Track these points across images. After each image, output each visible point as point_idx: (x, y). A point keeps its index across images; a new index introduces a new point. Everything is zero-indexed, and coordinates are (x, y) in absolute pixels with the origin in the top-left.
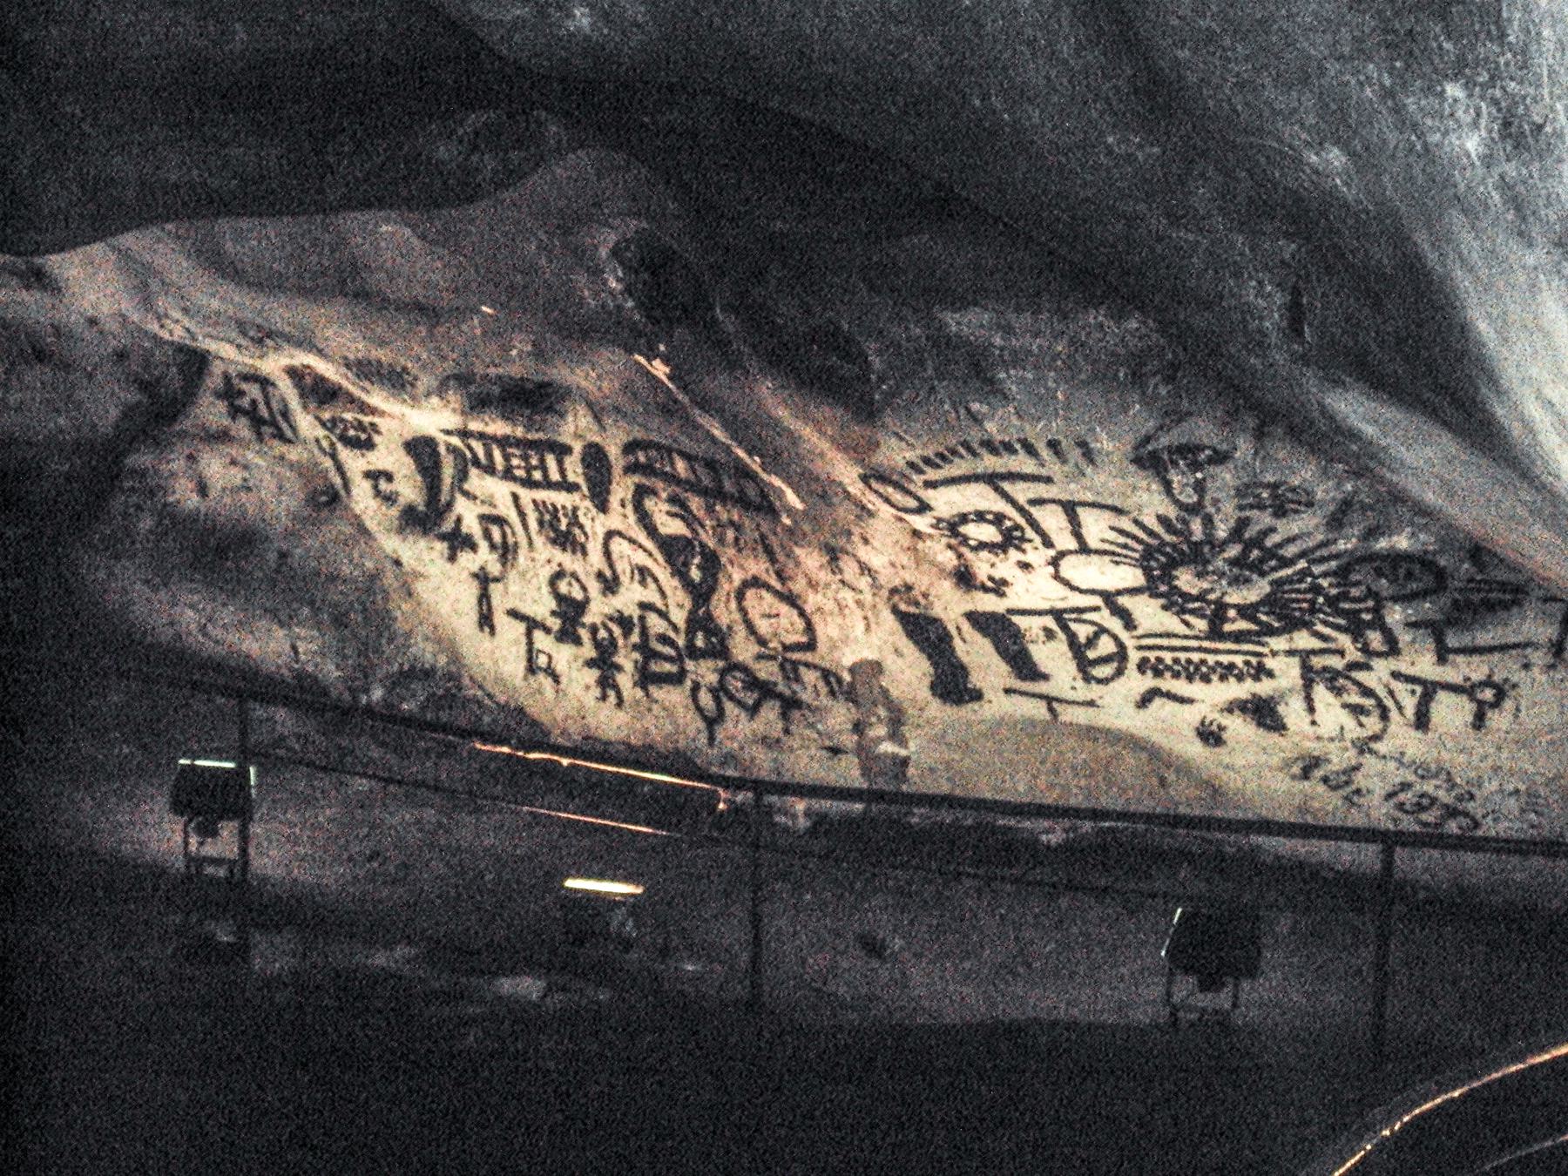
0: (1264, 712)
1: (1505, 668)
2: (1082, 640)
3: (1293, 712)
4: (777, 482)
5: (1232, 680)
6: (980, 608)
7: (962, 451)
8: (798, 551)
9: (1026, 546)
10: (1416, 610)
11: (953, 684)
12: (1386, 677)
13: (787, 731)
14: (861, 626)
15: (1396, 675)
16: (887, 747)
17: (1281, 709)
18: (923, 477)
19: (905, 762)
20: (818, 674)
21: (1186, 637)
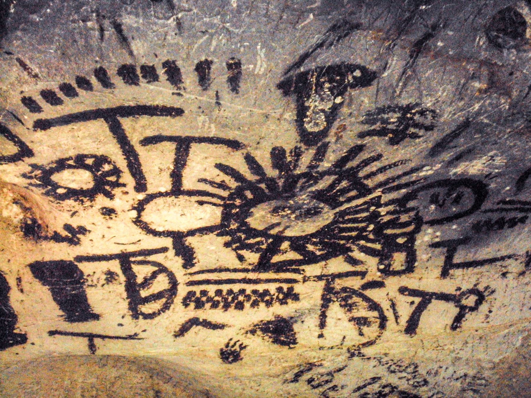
0: (281, 331)
1: (487, 278)
2: (140, 280)
3: (306, 331)
5: (262, 305)
7: (94, 80)
9: (117, 191)
10: (443, 232)
12: (394, 293)
15: (403, 290)
17: (296, 327)
18: (37, 116)
21: (235, 270)
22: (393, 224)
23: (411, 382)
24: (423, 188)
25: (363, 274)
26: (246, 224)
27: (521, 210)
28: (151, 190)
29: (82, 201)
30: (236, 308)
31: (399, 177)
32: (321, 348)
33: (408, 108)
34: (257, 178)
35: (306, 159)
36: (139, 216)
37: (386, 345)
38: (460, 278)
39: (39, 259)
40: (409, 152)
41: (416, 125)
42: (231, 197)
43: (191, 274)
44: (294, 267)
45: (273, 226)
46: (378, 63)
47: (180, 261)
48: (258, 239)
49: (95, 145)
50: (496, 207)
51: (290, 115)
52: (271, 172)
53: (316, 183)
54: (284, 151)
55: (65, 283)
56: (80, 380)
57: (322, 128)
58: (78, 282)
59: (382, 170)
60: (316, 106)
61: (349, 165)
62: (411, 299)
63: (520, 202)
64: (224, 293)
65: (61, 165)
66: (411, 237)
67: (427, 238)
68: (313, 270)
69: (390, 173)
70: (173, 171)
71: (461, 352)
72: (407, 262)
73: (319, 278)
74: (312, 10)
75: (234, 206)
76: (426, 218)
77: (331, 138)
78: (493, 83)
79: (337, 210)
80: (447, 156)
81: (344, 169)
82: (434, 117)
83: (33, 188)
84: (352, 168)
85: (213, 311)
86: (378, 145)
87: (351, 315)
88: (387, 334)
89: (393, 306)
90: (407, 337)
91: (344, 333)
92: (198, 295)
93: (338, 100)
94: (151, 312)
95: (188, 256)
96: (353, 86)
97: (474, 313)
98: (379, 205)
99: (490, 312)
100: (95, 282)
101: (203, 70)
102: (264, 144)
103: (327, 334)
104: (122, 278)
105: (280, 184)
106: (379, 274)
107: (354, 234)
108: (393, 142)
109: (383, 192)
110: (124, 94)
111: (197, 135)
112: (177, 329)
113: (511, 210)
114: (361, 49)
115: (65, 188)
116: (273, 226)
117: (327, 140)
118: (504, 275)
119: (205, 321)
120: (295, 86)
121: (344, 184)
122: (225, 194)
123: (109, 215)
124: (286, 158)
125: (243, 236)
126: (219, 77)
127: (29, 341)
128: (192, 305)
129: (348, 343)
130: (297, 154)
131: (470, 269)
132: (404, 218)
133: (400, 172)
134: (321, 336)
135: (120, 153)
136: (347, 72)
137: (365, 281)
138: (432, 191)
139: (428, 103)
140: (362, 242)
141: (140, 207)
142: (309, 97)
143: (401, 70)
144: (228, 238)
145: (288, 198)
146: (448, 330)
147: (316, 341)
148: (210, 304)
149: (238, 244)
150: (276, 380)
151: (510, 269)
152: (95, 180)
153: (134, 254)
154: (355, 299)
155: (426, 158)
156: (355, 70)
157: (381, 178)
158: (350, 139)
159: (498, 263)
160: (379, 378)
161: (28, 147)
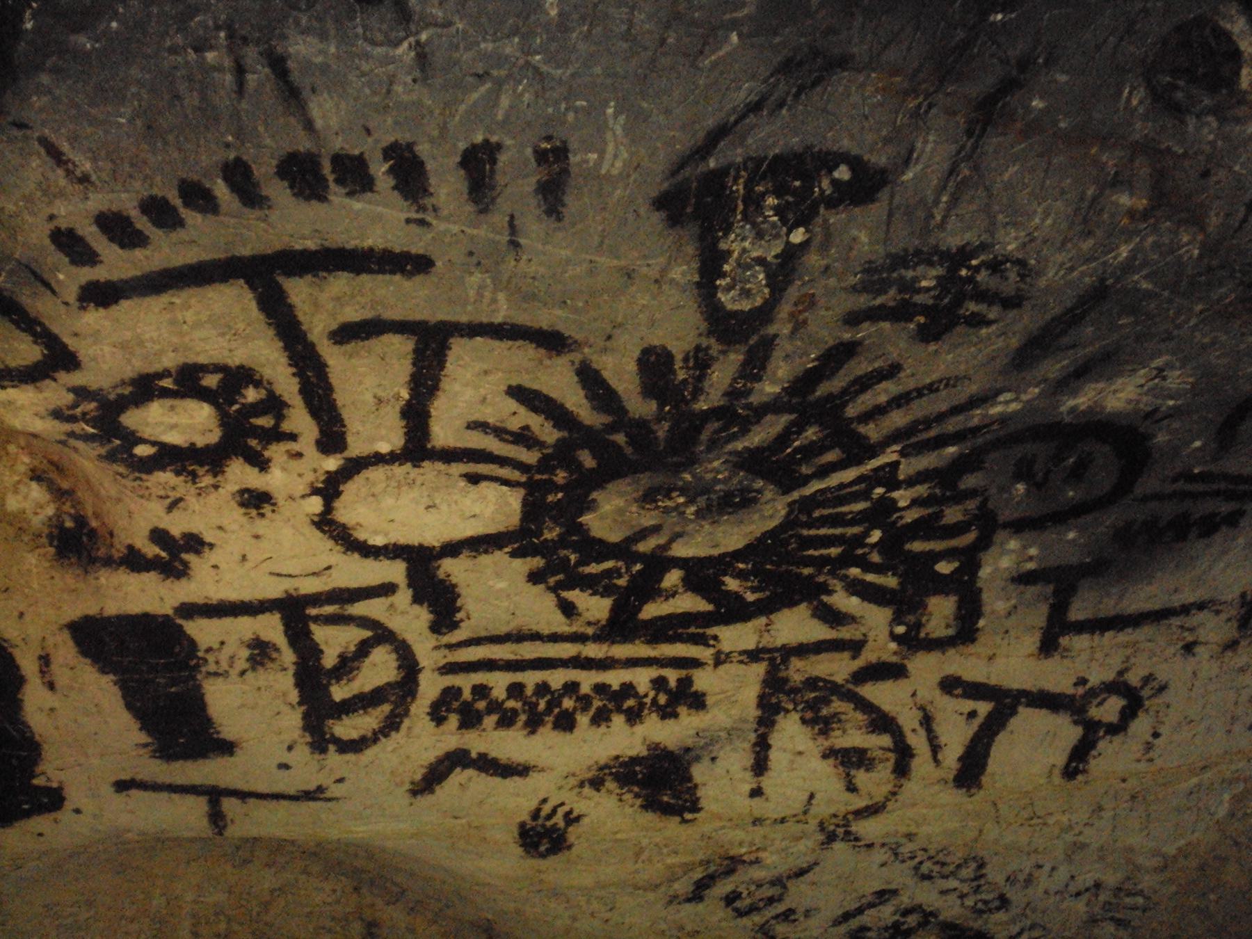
0: (662, 782)
1: (1149, 656)
2: (329, 660)
3: (721, 782)
5: (618, 720)
7: (221, 190)
9: (276, 452)
15: (950, 685)
17: (699, 772)
18: (87, 274)
21: (555, 638)
23: (969, 902)
24: (998, 444)
25: (855, 647)
27: (1229, 496)
28: (357, 447)
29: (194, 476)
31: (941, 417)
32: (757, 821)
35: (721, 376)
36: (328, 508)
37: (910, 813)
38: (1085, 656)
39: (93, 610)
40: (962, 359)
41: (983, 296)
42: (545, 464)
43: (450, 647)
44: (692, 630)
45: (643, 534)
46: (890, 150)
47: (423, 616)
48: (609, 564)
49: (222, 342)
50: (1169, 488)
51: (684, 272)
52: (639, 406)
53: (745, 431)
54: (669, 356)
55: (155, 669)
56: (189, 897)
57: (759, 301)
59: (900, 401)
60: (744, 250)
61: (822, 390)
62: (969, 705)
63: (1225, 477)
64: (529, 691)
65: (145, 388)
66: (970, 560)
68: (737, 637)
69: (920, 409)
70: (409, 403)
73: (753, 656)
75: (552, 487)
76: (1005, 515)
77: (780, 327)
79: (795, 495)
80: (1053, 368)
81: (811, 398)
82: (1022, 277)
83: (80, 444)
84: (830, 397)
85: (502, 733)
86: (891, 341)
87: (827, 744)
88: (912, 787)
89: (927, 721)
92: (467, 694)
93: (798, 236)
94: (355, 735)
95: (442, 603)
96: (832, 203)
97: (1118, 739)
99: (1156, 735)
100: (224, 665)
101: (478, 165)
102: (622, 339)
104: (288, 656)
105: (661, 434)
106: (893, 646)
107: (834, 551)
108: (928, 335)
109: (903, 453)
110: (293, 223)
111: (464, 319)
112: (418, 777)
113: (1204, 495)
114: (850, 117)
115: (154, 443)
116: (643, 534)
117: (771, 330)
118: (1189, 648)
120: (695, 204)
122: (530, 457)
123: (258, 507)
124: (674, 372)
125: (573, 558)
126: (517, 180)
127: (69, 805)
128: (454, 720)
129: (821, 809)
130: (701, 362)
132: (953, 515)
133: (944, 407)
134: (757, 792)
135: (284, 360)
137: (859, 663)
138: (1018, 451)
139: (1010, 244)
140: (855, 571)
141: (330, 489)
142: (728, 229)
143: (946, 166)
144: (537, 562)
145: (678, 468)
146: (1057, 779)
147: (744, 804)
148: (494, 718)
149: (561, 577)
150: (651, 896)
151: (1202, 634)
154: (837, 705)
156: (836, 166)
157: (898, 419)
158: (825, 328)
159: (1176, 621)
160: (895, 892)
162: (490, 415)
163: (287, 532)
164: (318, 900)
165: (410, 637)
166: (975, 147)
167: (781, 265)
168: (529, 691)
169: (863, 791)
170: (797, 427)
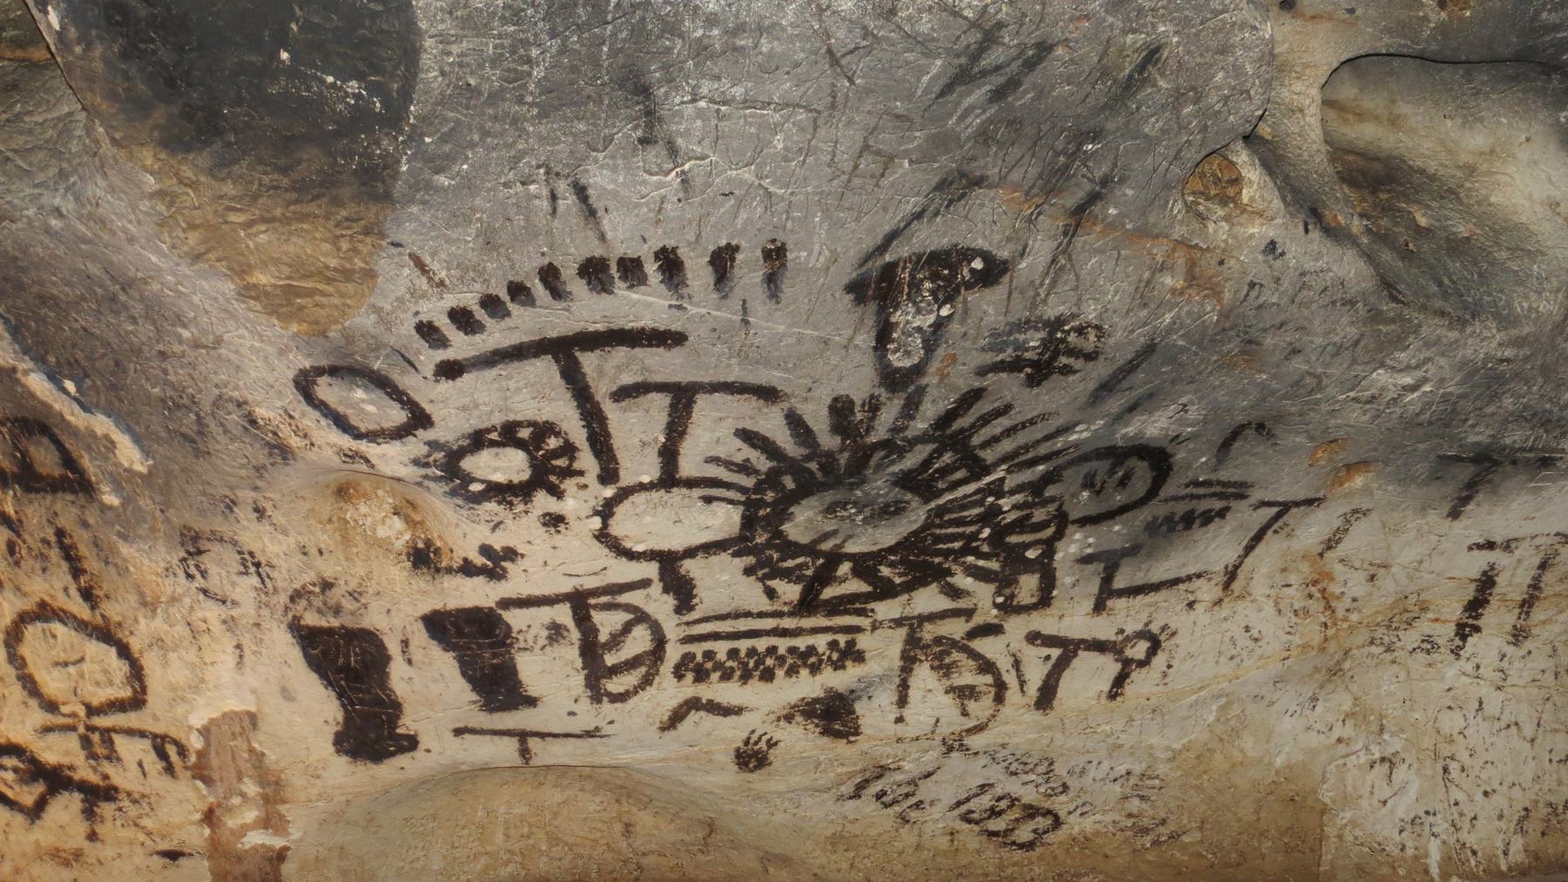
0: (833, 716)
1: (1163, 610)
3: (875, 714)
4: (101, 424)
5: (804, 672)
6: (453, 604)
8: (125, 550)
9: (569, 485)
11: (372, 729)
13: (92, 836)
14: (230, 659)
15: (1033, 638)
16: (256, 839)
17: (859, 707)
19: (281, 856)
20: (146, 744)
21: (761, 615)
22: (1020, 525)
23: (1042, 790)
24: (1072, 463)
25: (969, 613)
26: (779, 534)
27: (1221, 496)
28: (626, 479)
29: (511, 504)
30: (762, 678)
31: (1037, 443)
32: (899, 740)
33: (1058, 323)
34: (804, 451)
35: (888, 415)
36: (605, 525)
37: (1004, 729)
38: (1123, 613)
39: (439, 606)
40: (1056, 399)
41: (1071, 352)
42: (759, 488)
43: (688, 624)
44: (857, 605)
45: (826, 536)
46: (1011, 246)
47: (670, 601)
48: (800, 560)
49: (534, 403)
50: (1184, 492)
51: (866, 339)
52: (828, 441)
53: (901, 457)
54: (852, 403)
55: (480, 644)
56: (502, 810)
57: (916, 360)
58: (505, 645)
59: (1010, 432)
60: (908, 322)
61: (956, 426)
62: (1046, 651)
63: (1219, 483)
64: (743, 654)
65: (478, 441)
66: (1049, 547)
67: (1073, 549)
68: (886, 610)
69: (1022, 438)
70: (664, 445)
71: (1123, 736)
72: (1041, 589)
73: (898, 623)
74: (906, 154)
75: (761, 503)
76: (1074, 514)
77: (930, 379)
78: (1194, 278)
79: (933, 505)
80: (1115, 404)
81: (949, 432)
82: (1099, 338)
83: (431, 484)
84: (962, 430)
85: (724, 685)
86: (1009, 387)
87: (948, 683)
88: (1006, 710)
89: (1017, 664)
90: (1037, 716)
91: (936, 714)
92: (699, 658)
93: (945, 312)
94: (621, 690)
95: (682, 592)
96: (969, 286)
97: (1144, 670)
98: (1000, 494)
99: (1169, 667)
100: (530, 642)
101: (722, 261)
102: (817, 392)
103: (912, 715)
104: (575, 635)
105: (843, 462)
106: (995, 612)
107: (957, 545)
108: (1033, 382)
109: (1009, 471)
110: (588, 310)
111: (707, 380)
112: (666, 718)
113: (1205, 496)
114: (982, 225)
115: (483, 482)
116: (826, 536)
117: (924, 381)
118: (1191, 605)
119: (710, 702)
120: (877, 288)
121: (948, 458)
122: (748, 482)
123: (555, 526)
124: (853, 413)
125: (775, 556)
126: (749, 272)
127: (421, 746)
128: (690, 677)
129: (944, 730)
130: (873, 407)
131: (1140, 597)
132: (1039, 515)
133: (1040, 436)
134: (900, 720)
135: (577, 416)
136: (960, 262)
137: (971, 625)
138: (1086, 468)
139: (1091, 313)
140: (970, 559)
141: (606, 511)
142: (897, 307)
143: (1049, 258)
144: (750, 560)
145: (852, 487)
146: (1104, 700)
147: (892, 729)
148: (718, 674)
149: (766, 570)
150: (825, 796)
151: (1199, 595)
152: (532, 466)
153: (595, 592)
154: (956, 655)
155: (1081, 409)
156: (973, 259)
157: (1007, 446)
158: (963, 380)
159: (1181, 586)
160: (991, 785)
161: (423, 410)
162: (722, 452)
163: (576, 543)
164: (591, 809)
165: (660, 617)
166: (1069, 243)
167: (934, 333)
168: (743, 654)
169: (973, 715)
170: (939, 453)
